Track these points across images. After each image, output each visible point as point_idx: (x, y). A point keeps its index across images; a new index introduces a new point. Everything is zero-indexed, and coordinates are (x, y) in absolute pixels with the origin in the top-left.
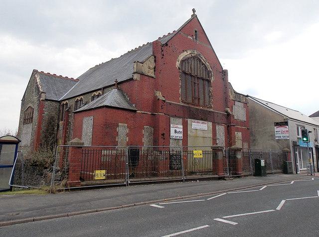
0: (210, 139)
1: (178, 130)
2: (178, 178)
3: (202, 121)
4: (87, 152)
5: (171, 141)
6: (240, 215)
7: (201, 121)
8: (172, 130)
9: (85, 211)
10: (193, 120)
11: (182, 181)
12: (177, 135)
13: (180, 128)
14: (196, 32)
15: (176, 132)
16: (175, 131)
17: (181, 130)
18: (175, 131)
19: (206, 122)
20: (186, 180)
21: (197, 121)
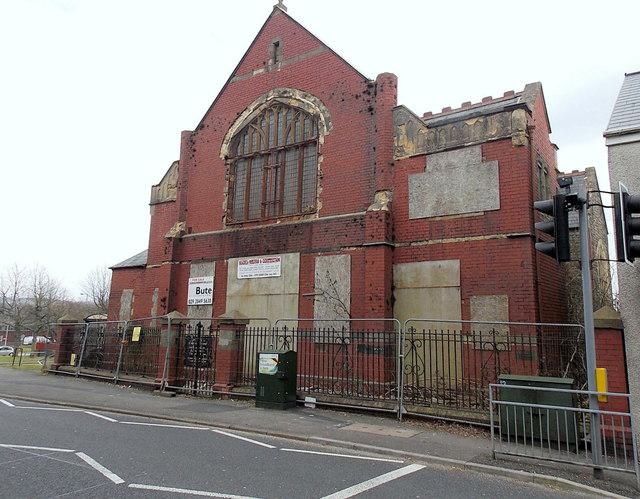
0: (444, 294)
1: (202, 287)
2: (104, 374)
3: (265, 257)
4: (452, 338)
5: (190, 309)
6: (145, 487)
7: (260, 258)
8: (192, 289)
9: (366, 446)
10: (240, 260)
11: (112, 381)
12: (201, 297)
13: (208, 282)
14: (277, 45)
15: (198, 291)
16: (198, 289)
17: (211, 286)
18: (198, 289)
19: (279, 256)
20: (118, 382)
21: (249, 259)
